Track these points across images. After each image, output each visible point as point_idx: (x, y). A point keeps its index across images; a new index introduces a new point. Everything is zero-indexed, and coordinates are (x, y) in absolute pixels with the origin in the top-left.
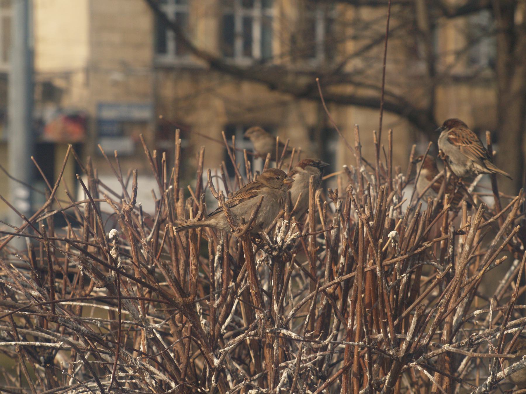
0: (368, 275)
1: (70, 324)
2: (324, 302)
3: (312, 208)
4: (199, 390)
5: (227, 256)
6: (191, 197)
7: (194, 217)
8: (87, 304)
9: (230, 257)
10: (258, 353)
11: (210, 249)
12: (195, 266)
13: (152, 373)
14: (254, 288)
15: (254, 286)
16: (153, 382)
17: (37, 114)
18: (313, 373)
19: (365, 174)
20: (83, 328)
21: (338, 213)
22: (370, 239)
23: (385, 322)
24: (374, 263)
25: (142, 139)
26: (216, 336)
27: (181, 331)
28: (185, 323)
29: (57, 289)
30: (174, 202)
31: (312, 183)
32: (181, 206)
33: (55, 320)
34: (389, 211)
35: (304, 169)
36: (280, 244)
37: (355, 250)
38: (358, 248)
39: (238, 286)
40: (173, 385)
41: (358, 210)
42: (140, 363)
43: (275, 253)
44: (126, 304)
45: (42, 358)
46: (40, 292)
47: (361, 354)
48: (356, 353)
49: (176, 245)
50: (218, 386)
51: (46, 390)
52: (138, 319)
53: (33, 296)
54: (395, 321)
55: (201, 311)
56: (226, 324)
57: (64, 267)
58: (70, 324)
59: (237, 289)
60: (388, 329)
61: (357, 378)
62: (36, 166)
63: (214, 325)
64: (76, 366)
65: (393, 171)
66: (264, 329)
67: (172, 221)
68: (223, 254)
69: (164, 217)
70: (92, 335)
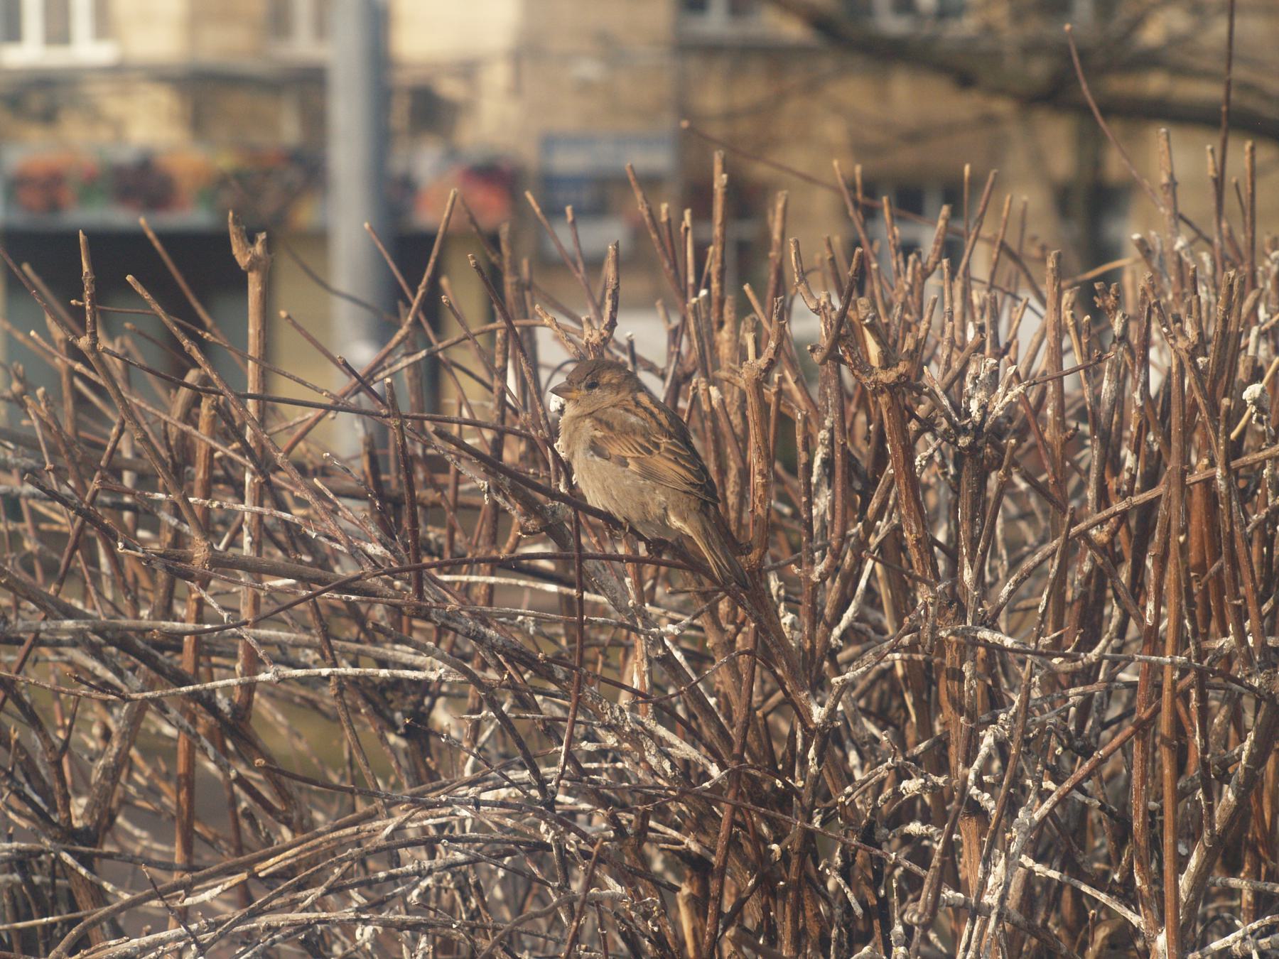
0: (1197, 497)
2: (1087, 567)
4: (779, 783)
5: (842, 454)
6: (752, 316)
7: (758, 354)
8: (502, 580)
9: (848, 457)
10: (925, 697)
11: (799, 438)
12: (764, 476)
13: (660, 742)
14: (914, 528)
16: (667, 765)
17: (398, 164)
18: (1062, 740)
20: (491, 633)
22: (1199, 400)
23: (1239, 607)
24: (1212, 464)
25: (647, 220)
26: (818, 653)
27: (733, 641)
28: (743, 623)
29: (433, 547)
30: (712, 330)
32: (730, 340)
33: (423, 614)
34: (1248, 335)
36: (978, 419)
37: (1163, 435)
38: (1170, 430)
39: (870, 529)
40: (714, 771)
41: (1169, 328)
42: (632, 718)
43: (964, 441)
44: (595, 575)
45: (398, 715)
46: (385, 546)
47: (1179, 687)
48: (1167, 685)
49: (716, 430)
50: (825, 772)
51: (411, 786)
52: (627, 610)
53: (369, 556)
54: (1263, 603)
55: (782, 592)
56: (843, 624)
57: (449, 493)
59: (868, 536)
60: (1247, 625)
61: (1170, 746)
63: (813, 625)
64: (477, 728)
65: (1257, 245)
66: (934, 629)
67: (706, 375)
68: (833, 451)
69: (689, 367)
70: (515, 650)
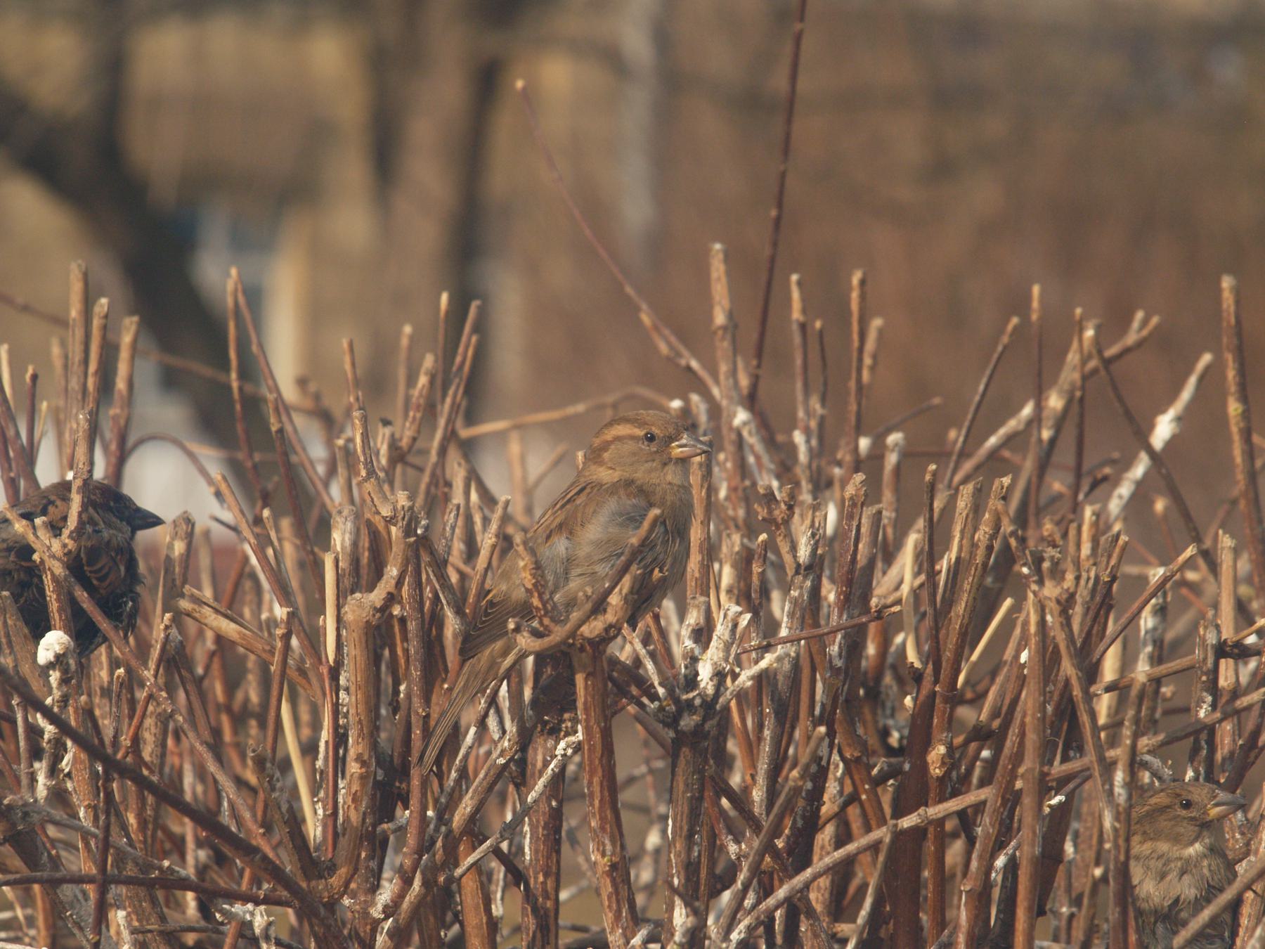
3: (699, 558)
12: (363, 763)
14: (609, 848)
15: (607, 842)
19: (750, 433)
21: (805, 577)
36: (710, 690)
44: (72, 907)
62: (566, 420)
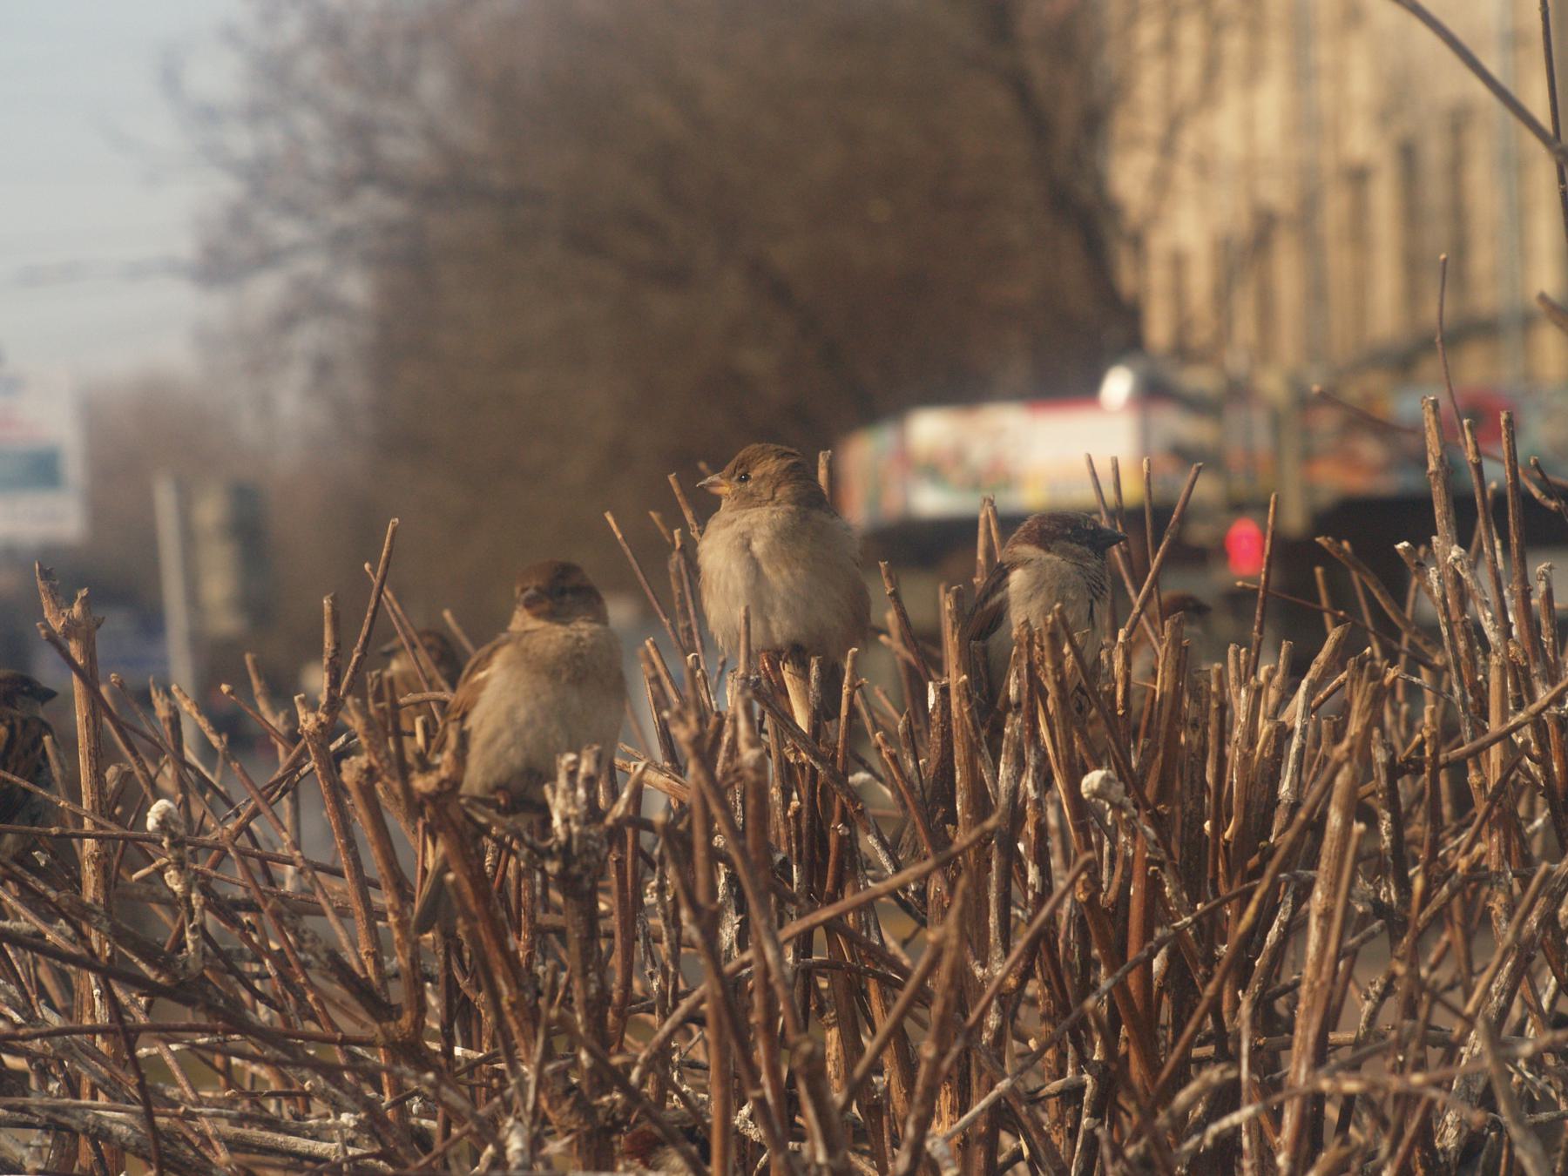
1: (74, 1117)
31: (950, 612)
35: (1048, 550)
58: (74, 1117)
